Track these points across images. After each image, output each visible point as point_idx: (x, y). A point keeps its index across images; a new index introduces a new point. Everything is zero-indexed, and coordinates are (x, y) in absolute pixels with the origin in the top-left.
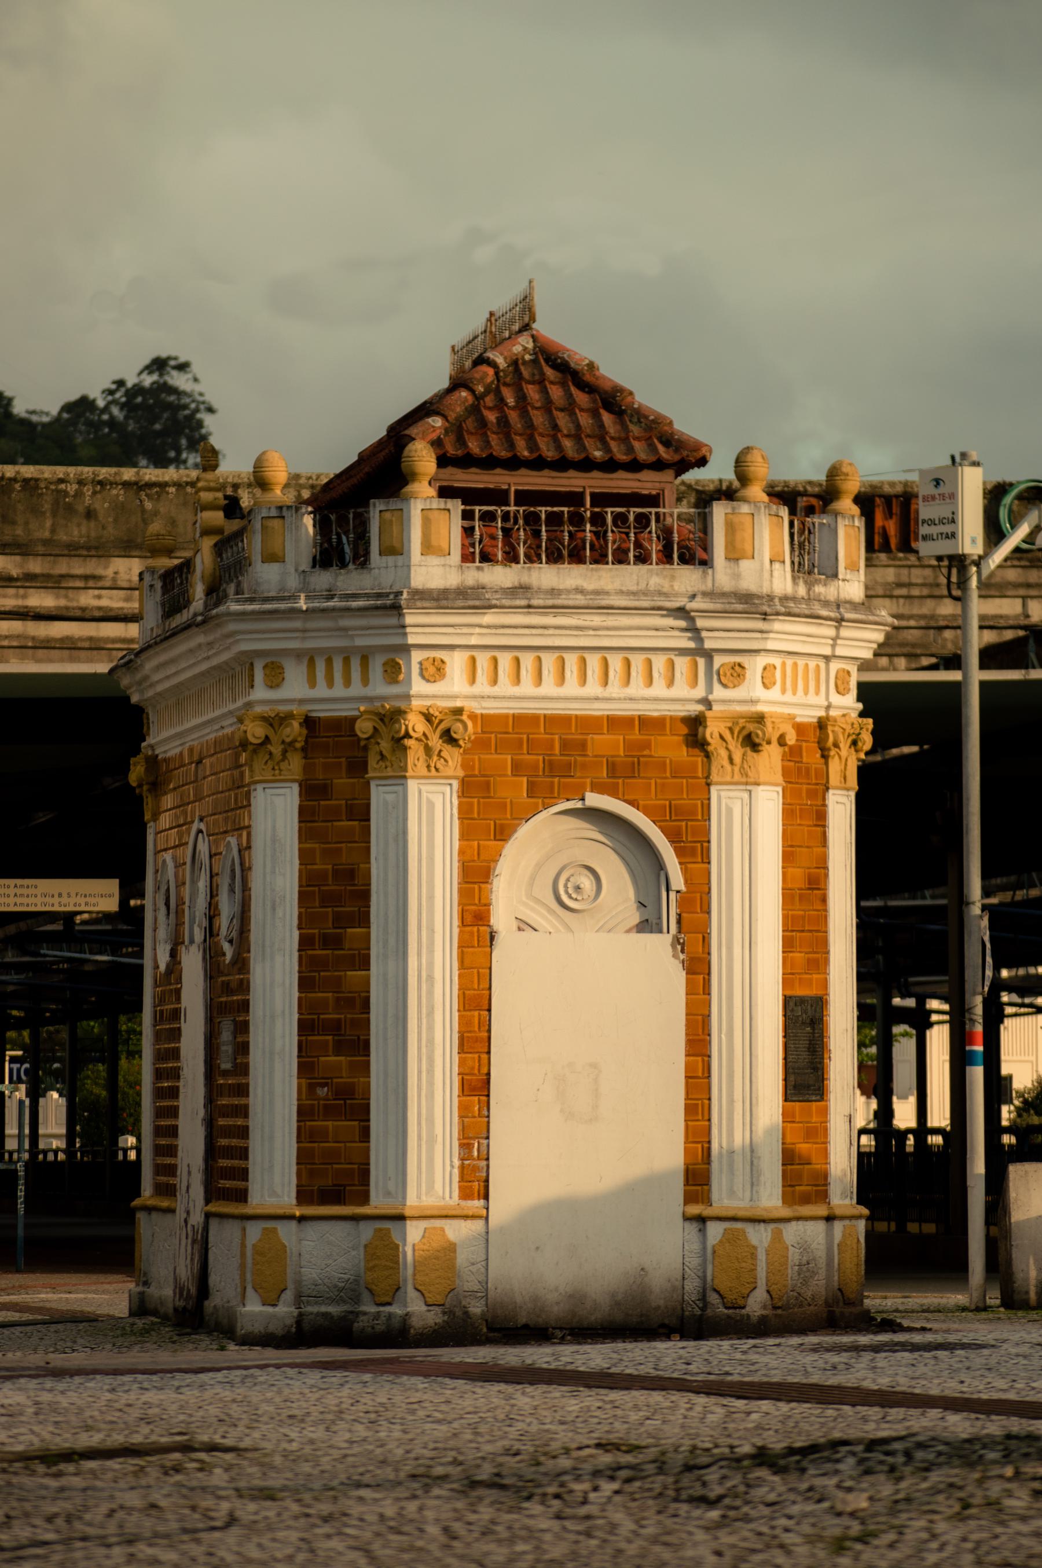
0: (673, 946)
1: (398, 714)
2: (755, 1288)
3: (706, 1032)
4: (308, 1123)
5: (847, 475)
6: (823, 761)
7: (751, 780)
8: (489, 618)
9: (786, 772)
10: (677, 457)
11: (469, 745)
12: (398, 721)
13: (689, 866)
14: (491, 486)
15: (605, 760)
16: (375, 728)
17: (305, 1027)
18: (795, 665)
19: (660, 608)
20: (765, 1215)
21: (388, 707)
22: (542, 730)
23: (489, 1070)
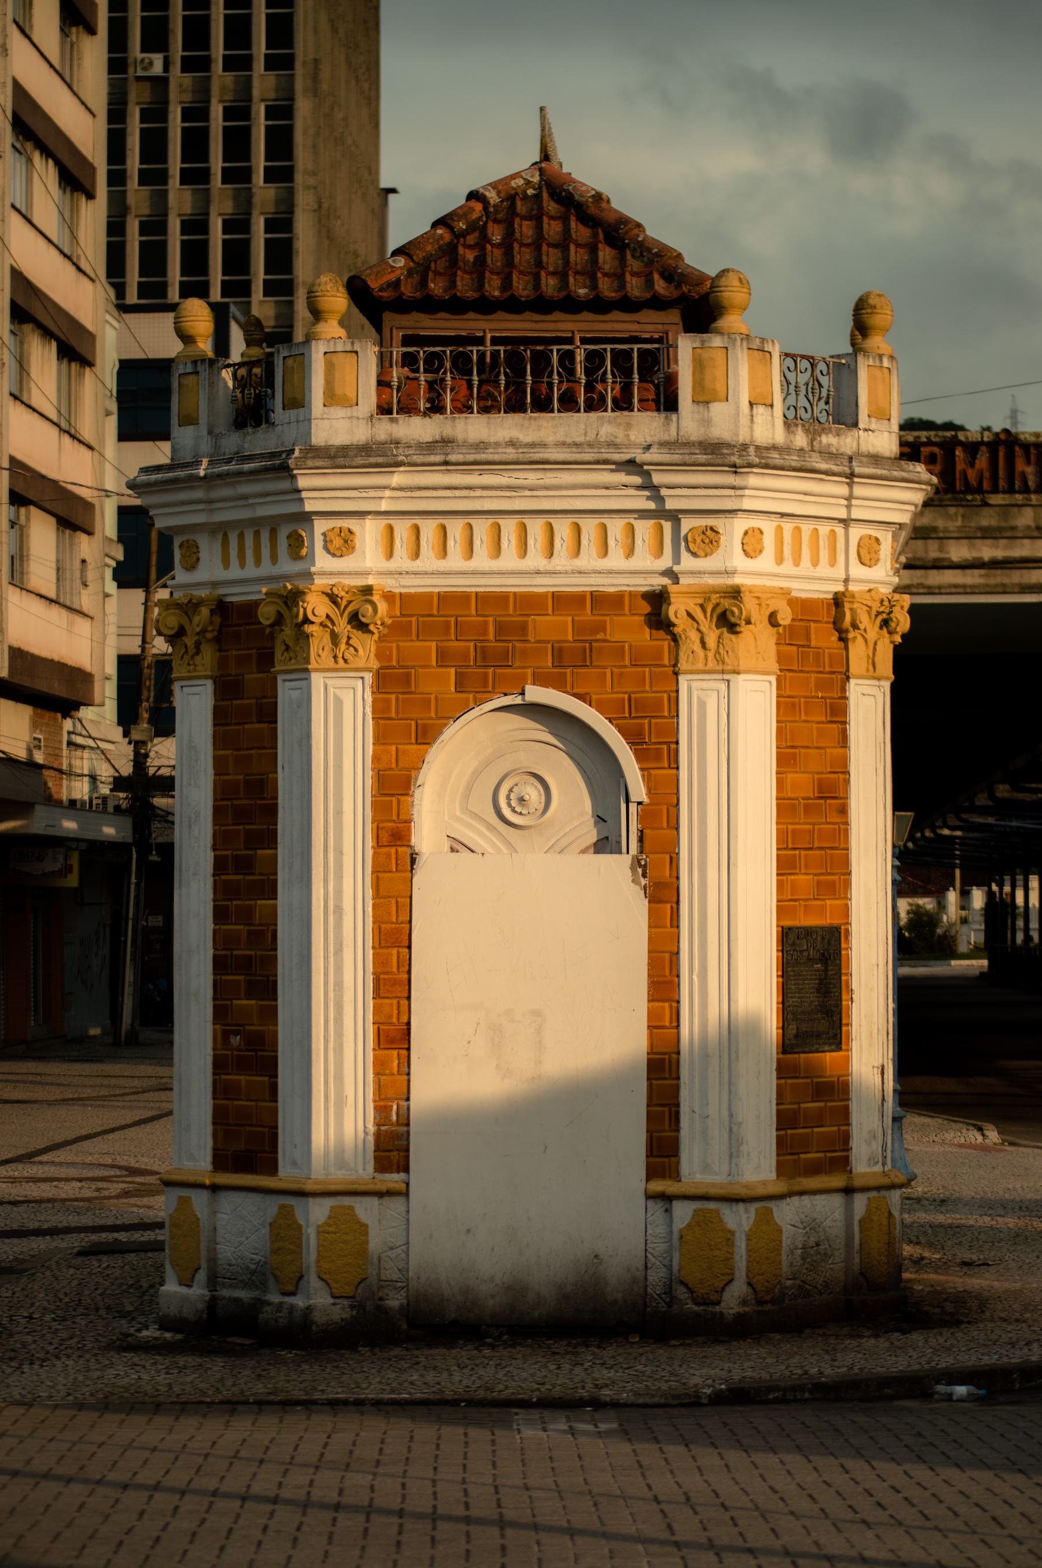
0: (633, 869)
1: (294, 597)
2: (732, 1280)
3: (675, 972)
4: (223, 1077)
5: (875, 307)
7: (730, 668)
8: (397, 479)
9: (781, 658)
10: (676, 294)
11: (386, 631)
12: (297, 605)
13: (653, 772)
15: (550, 646)
16: (279, 613)
17: (220, 965)
18: (798, 530)
20: (743, 1192)
21: (289, 587)
22: (473, 612)
23: (409, 1018)
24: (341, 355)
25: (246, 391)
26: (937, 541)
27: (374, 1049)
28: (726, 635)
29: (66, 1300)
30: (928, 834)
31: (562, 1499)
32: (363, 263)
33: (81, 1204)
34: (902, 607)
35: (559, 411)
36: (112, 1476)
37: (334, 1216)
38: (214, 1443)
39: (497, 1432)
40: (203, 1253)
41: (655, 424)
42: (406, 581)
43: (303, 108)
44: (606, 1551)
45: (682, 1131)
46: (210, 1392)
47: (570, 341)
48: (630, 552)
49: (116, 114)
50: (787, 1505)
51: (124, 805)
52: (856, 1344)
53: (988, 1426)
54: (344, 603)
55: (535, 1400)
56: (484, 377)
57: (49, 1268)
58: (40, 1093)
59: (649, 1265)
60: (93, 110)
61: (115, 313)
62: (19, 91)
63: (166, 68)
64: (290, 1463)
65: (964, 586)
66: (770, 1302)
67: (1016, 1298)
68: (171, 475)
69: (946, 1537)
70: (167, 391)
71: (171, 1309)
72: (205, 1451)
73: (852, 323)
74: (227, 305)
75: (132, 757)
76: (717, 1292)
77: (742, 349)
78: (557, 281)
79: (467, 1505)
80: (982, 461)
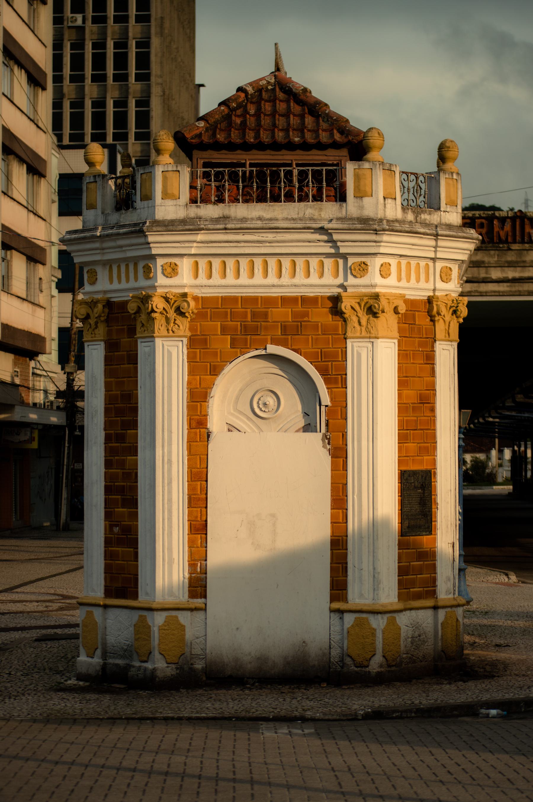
0: (323, 440)
1: (146, 299)
2: (374, 655)
3: (345, 494)
4: (110, 548)
5: (449, 147)
6: (432, 323)
7: (373, 335)
8: (200, 237)
9: (400, 330)
10: (345, 140)
11: (194, 316)
12: (148, 303)
13: (333, 390)
14: (235, 161)
15: (280, 324)
17: (108, 490)
19: (309, 228)
20: (381, 609)
21: (144, 293)
22: (240, 306)
24: (171, 173)
25: (121, 191)
26: (484, 268)
27: (188, 534)
28: (372, 318)
29: (29, 664)
30: (481, 420)
31: (284, 769)
32: (187, 123)
33: (38, 614)
34: (463, 304)
35: (284, 202)
36: (50, 757)
37: (167, 621)
38: (104, 740)
39: (251, 734)
40: (100, 640)
41: (334, 209)
42: (205, 290)
43: (155, 42)
44: (306, 797)
45: (348, 577)
46: (102, 713)
47: (290, 165)
48: (321, 275)
49: (58, 46)
50: (401, 773)
51: (62, 406)
52: (439, 687)
53: (507, 731)
54: (172, 302)
55: (271, 717)
56: (245, 184)
57: (20, 648)
58: (17, 556)
59: (332, 647)
60: (45, 44)
61: (57, 150)
62: (6, 33)
63: (84, 22)
64: (143, 750)
65: (499, 292)
66: (395, 666)
67: (523, 664)
68: (82, 235)
69: (483, 789)
70: (81, 190)
71: (83, 670)
72: (99, 744)
73: (437, 156)
74: (115, 145)
75: (66, 381)
76: (367, 660)
77: (380, 169)
78: (283, 134)
79: (234, 773)
80: (508, 227)
